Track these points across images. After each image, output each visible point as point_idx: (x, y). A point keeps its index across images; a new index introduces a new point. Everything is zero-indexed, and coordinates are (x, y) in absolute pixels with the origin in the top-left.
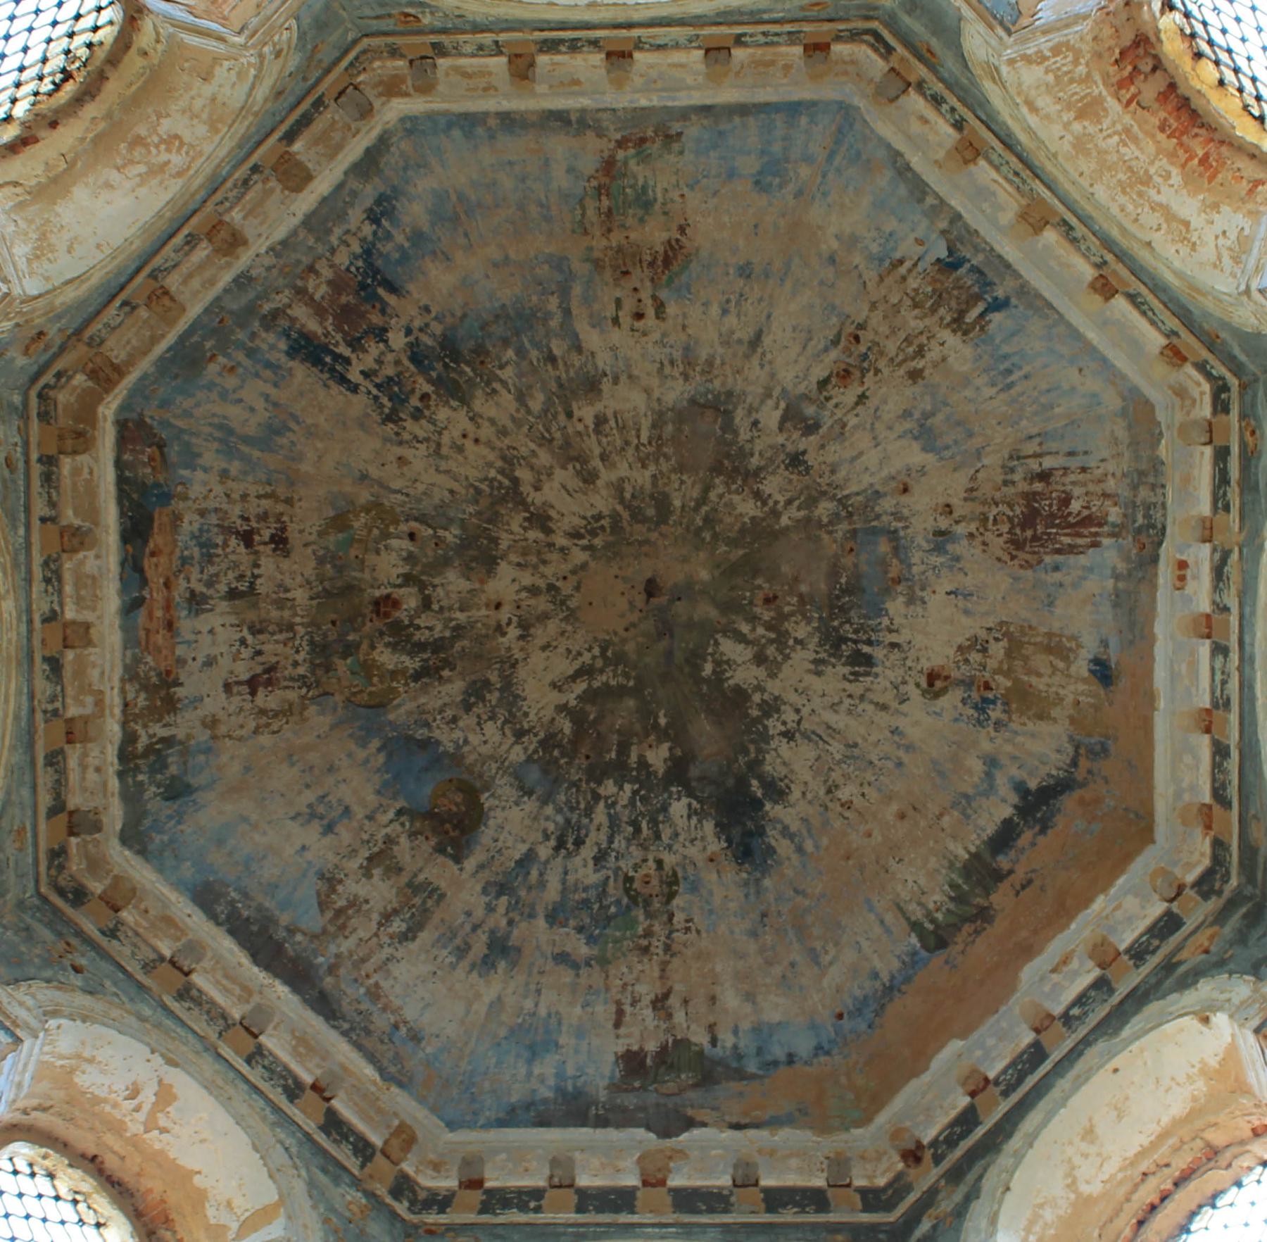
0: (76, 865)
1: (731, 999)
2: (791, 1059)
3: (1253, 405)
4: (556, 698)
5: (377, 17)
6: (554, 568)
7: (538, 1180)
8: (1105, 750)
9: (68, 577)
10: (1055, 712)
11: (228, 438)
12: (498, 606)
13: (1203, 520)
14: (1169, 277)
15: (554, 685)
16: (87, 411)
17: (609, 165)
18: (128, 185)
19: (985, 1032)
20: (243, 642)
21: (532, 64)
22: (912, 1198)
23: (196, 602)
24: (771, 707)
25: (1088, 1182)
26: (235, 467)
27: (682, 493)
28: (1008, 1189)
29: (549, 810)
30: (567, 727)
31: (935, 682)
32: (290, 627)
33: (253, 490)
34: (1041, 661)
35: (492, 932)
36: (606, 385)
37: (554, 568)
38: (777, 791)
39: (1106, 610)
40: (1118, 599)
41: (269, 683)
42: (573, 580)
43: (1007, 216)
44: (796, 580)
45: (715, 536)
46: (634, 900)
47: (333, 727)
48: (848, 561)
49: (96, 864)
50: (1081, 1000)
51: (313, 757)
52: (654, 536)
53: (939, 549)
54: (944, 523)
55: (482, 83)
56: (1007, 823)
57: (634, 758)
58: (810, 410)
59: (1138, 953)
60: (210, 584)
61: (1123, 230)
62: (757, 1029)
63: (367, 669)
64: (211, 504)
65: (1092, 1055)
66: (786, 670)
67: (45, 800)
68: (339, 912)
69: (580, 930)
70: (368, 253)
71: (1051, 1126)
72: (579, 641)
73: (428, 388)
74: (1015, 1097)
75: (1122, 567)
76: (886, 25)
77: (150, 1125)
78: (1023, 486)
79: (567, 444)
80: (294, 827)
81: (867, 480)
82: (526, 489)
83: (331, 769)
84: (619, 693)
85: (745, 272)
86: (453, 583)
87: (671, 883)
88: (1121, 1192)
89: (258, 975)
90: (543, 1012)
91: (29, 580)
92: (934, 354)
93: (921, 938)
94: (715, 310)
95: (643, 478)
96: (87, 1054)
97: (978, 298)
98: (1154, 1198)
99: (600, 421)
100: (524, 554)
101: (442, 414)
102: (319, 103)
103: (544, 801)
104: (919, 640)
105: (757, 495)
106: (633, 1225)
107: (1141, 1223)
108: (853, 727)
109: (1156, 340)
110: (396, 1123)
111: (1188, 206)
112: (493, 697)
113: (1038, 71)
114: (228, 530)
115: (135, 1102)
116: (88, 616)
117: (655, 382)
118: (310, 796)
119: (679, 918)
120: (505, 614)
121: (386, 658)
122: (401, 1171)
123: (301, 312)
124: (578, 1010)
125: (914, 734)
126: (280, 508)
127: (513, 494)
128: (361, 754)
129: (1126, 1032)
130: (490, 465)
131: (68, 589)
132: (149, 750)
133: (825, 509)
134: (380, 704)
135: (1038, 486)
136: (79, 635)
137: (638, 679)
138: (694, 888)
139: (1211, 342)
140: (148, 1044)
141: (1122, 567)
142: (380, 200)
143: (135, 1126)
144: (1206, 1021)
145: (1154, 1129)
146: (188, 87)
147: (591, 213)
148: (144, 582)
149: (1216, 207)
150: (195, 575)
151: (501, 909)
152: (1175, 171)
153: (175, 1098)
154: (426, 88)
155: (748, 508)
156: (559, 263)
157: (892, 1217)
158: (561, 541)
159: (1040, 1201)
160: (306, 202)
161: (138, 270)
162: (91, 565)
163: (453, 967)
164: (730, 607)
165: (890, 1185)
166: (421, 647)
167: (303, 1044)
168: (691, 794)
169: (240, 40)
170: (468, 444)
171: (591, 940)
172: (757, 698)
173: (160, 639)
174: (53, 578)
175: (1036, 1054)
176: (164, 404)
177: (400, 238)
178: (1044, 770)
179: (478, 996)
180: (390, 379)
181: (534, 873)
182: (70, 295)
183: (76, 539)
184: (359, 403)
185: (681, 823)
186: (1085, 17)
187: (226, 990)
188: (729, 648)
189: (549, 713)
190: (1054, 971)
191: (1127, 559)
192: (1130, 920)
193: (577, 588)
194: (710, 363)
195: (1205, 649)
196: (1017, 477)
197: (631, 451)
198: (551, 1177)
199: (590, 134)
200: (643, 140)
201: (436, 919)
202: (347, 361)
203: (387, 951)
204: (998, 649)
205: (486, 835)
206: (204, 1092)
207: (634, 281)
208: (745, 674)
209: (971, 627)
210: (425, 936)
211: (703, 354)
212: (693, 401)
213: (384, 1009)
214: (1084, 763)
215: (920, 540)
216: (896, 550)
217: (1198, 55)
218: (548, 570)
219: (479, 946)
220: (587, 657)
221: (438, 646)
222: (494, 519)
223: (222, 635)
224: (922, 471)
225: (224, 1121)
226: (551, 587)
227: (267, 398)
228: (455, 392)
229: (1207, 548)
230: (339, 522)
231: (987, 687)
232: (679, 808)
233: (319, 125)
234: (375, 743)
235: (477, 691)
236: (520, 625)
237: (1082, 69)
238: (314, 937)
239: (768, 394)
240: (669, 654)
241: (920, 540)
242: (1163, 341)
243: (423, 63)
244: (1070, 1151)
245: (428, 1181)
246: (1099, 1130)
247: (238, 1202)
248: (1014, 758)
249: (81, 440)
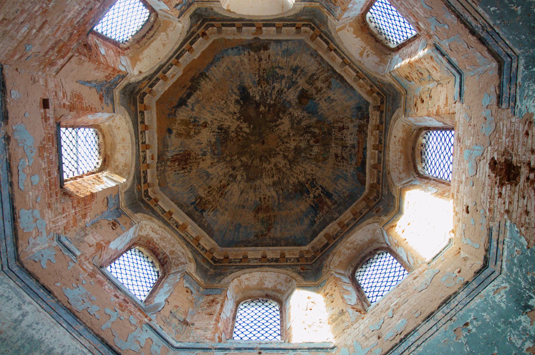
0: (379, 99)
1: (246, 60)
2: (232, 49)
3: (139, 194)
4: (283, 121)
5: (308, 269)
6: (283, 147)
7: (284, 29)
8: (169, 115)
9: (377, 159)
10: (179, 121)
11: (346, 179)
12: (294, 140)
13: (149, 168)
14: (156, 220)
15: (283, 123)
16: (371, 191)
17: (269, 230)
18: (357, 241)
19: (189, 61)
20: (345, 137)
21: (281, 256)
22: (203, 27)
23: (353, 146)
24: (238, 119)
26: (345, 172)
27: (257, 162)
29: (284, 98)
30: (281, 115)
31: (205, 125)
32: (335, 139)
33: (341, 167)
34: (183, 132)
35: (296, 74)
36: (271, 184)
37: (283, 147)
38: (237, 102)
39: (169, 144)
40: (167, 146)
41: (340, 128)
42: (279, 145)
43: (189, 226)
44: (234, 144)
45: (250, 153)
46: (267, 80)
47: (328, 117)
48: (223, 149)
49: (375, 99)
50: (169, 69)
51: (332, 112)
52: (263, 153)
53: (205, 152)
54: (204, 157)
55: (290, 253)
56: (189, 99)
57: (267, 108)
58: (231, 179)
59: (158, 79)
60: (350, 150)
61: (165, 230)
62: (240, 55)
63: (320, 129)
64: (350, 166)
65: (165, 60)
66: (236, 126)
67: (384, 115)
68: (327, 81)
69: (278, 74)
70: (316, 214)
72: (278, 132)
73: (306, 185)
74: (182, 49)
75: (167, 153)
76: (212, 264)
77: (365, 48)
78: (187, 166)
79: (280, 172)
80: (336, 98)
81: (220, 165)
82: (288, 163)
83: (328, 109)
84: (269, 122)
85: (243, 207)
86: (303, 145)
87: (259, 83)
88: (156, 33)
89: (343, 74)
90: (285, 58)
91: (384, 162)
92: (206, 192)
93: (206, 74)
94: (250, 199)
95: (265, 165)
97: (197, 204)
99: (273, 177)
101: (304, 179)
102: (322, 251)
103: (285, 100)
104: (208, 133)
105: (242, 161)
107: (152, 26)
108: (221, 115)
109: (160, 203)
111: (152, 235)
112: (295, 121)
113: (181, 261)
114: (347, 160)
116: (373, 151)
117: (262, 184)
118: (333, 104)
119: (257, 76)
120: (293, 138)
121: (317, 131)
123: (330, 204)
124: (278, 58)
125: (209, 114)
126: (336, 163)
127: (290, 162)
128: (322, 112)
129: (158, 66)
130: (295, 169)
131: (377, 157)
132: (364, 118)
133: (228, 159)
134: (318, 121)
135: (185, 166)
136: (375, 147)
137: (266, 124)
138: (254, 82)
139: (148, 206)
141: (167, 153)
142: (313, 225)
145: (151, 47)
146: (344, 259)
147: (273, 220)
148: (363, 153)
149: (147, 235)
150: (353, 152)
151: (294, 78)
152: (155, 241)
154: (301, 252)
155: (244, 159)
156: (280, 209)
157: (207, 23)
158: (281, 153)
160: (325, 231)
161: (384, 151)
162: (372, 161)
163: (304, 68)
164: (247, 139)
166: (310, 132)
167: (333, 59)
168: (255, 101)
169: (332, 272)
170: (299, 173)
171: (276, 72)
172: (242, 120)
173: (361, 141)
174: (379, 160)
175: (178, 58)
176: (357, 187)
177: (310, 216)
178: (182, 109)
179: (299, 61)
180: (314, 187)
181: (287, 85)
182: (370, 220)
183: (374, 167)
184: (320, 183)
185: (257, 95)
186: (173, 274)
187: (349, 71)
188: (248, 131)
189: (284, 118)
190: (175, 75)
191: (166, 155)
192: (160, 86)
193: (278, 143)
194: (251, 188)
195: (147, 142)
196: (189, 168)
197: (267, 170)
199: (272, 237)
200: (262, 236)
201: (308, 77)
202: (321, 192)
203: (318, 72)
204: (192, 133)
205: (297, 94)
207: (265, 205)
208: (244, 125)
209: (197, 137)
210: (309, 74)
211: (252, 190)
212: (254, 180)
213: (318, 61)
214: (173, 112)
215: (209, 154)
216: (214, 151)
217: (152, 262)
218: (284, 147)
219: (299, 72)
220: (276, 129)
221: (306, 132)
222: (294, 158)
223: (349, 139)
224: (209, 167)
226: (283, 143)
227: (338, 186)
228: (301, 184)
229: (148, 162)
230: (325, 159)
231: (194, 125)
232: (258, 98)
233: (322, 246)
234: (320, 113)
235: (299, 122)
236: (290, 136)
237: (174, 261)
238: (332, 77)
239: (239, 182)
240: (260, 129)
241: (209, 154)
242: (158, 203)
243: (301, 256)
244: (168, 41)
245: (308, 29)
246: (162, 46)
247: (346, 32)
248: (188, 111)
249: (372, 186)
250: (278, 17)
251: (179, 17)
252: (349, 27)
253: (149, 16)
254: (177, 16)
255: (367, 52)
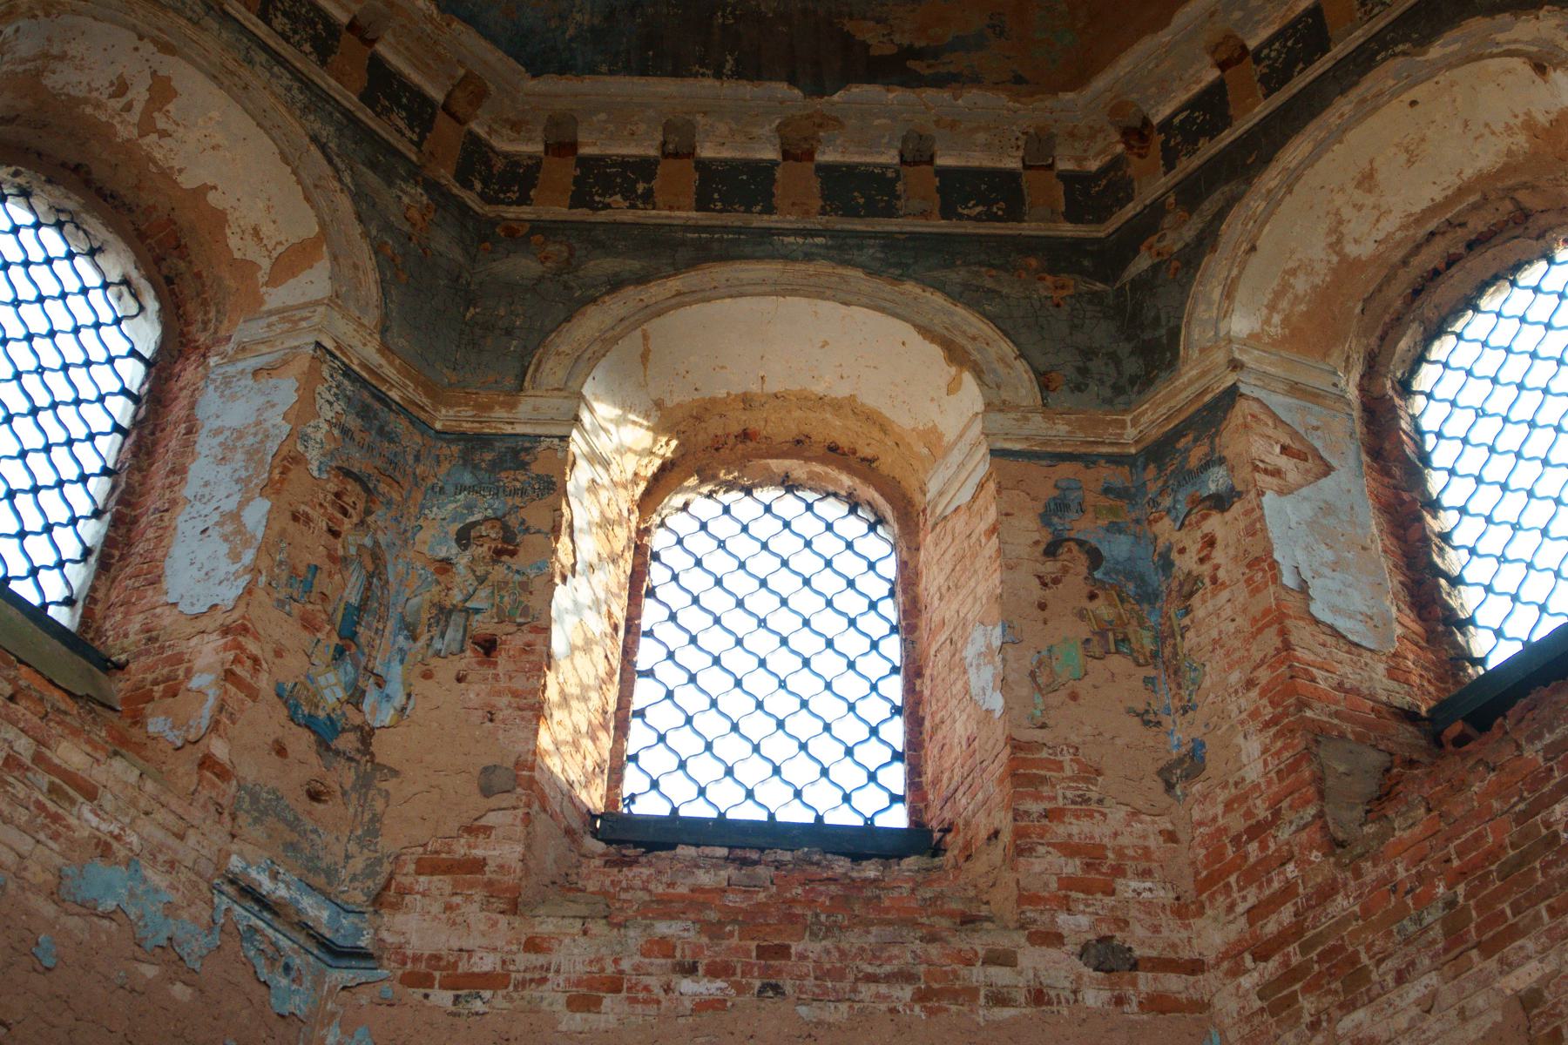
22: (1131, 210)
25: (1356, 241)
28: (1253, 248)
71: (1320, 165)
77: (146, 126)
96: (55, 51)
98: (1437, 263)
100: (714, 931)
106: (768, 232)
107: (1417, 293)
110: (461, 72)
115: (123, 101)
122: (470, 133)
129: (1435, 52)
140: (134, 28)
143: (125, 131)
144: (1540, 69)
153: (175, 94)
157: (1101, 231)
159: (1291, 264)
165: (1103, 171)
198: (664, 144)
206: (213, 87)
225: (240, 122)
244: (1339, 200)
246: (1379, 177)
247: (267, 229)
250: (674, 284)
251: (1232, 394)
252: (254, 266)
253: (1420, 359)
254: (1242, 408)
255: (128, 108)
